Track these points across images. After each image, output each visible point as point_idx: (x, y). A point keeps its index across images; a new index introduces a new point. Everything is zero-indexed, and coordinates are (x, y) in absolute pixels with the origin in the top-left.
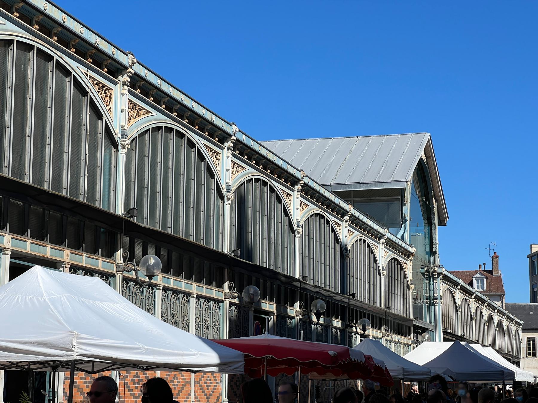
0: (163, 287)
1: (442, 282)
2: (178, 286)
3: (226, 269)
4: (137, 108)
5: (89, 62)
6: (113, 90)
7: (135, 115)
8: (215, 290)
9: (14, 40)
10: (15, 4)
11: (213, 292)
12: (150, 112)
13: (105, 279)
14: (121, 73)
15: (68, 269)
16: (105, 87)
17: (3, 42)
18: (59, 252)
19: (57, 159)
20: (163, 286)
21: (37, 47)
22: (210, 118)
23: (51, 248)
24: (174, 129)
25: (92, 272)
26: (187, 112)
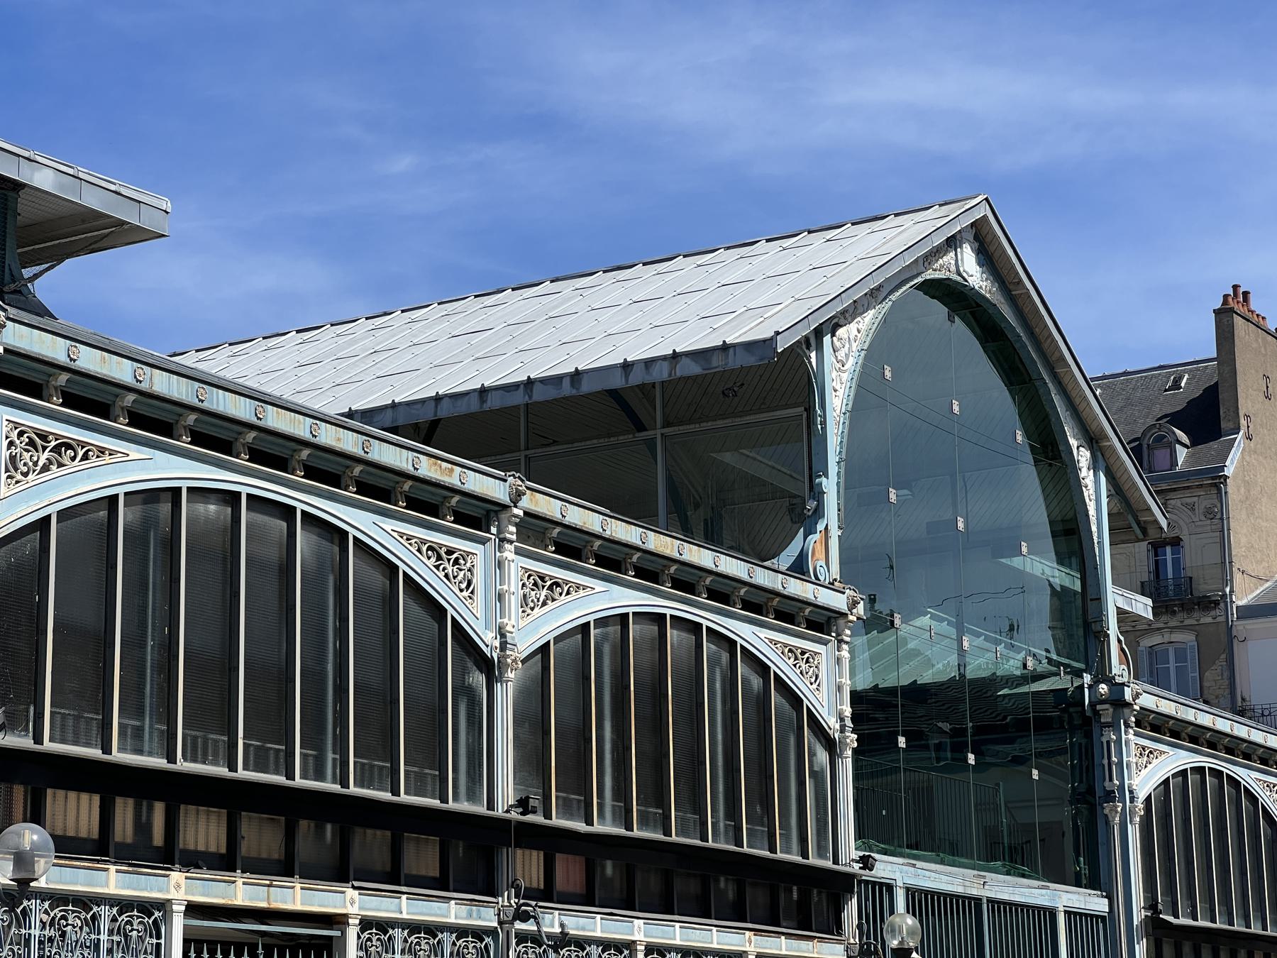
0: (186, 906)
1: (516, 553)
2: (320, 906)
3: (505, 850)
4: (1147, 753)
5: (400, 508)
6: (476, 554)
7: (1144, 763)
8: (240, 881)
9: (181, 488)
10: (118, 400)
11: (595, 923)
12: (585, 587)
13: (613, 952)
14: (495, 518)
15: (182, 914)
16: (806, 653)
17: (618, 617)
18: (130, 877)
19: (20, 650)
20: (186, 902)
21: (302, 511)
22: (1210, 723)
23: (407, 899)
24: (666, 615)
25: (434, 930)
26: (54, 374)
